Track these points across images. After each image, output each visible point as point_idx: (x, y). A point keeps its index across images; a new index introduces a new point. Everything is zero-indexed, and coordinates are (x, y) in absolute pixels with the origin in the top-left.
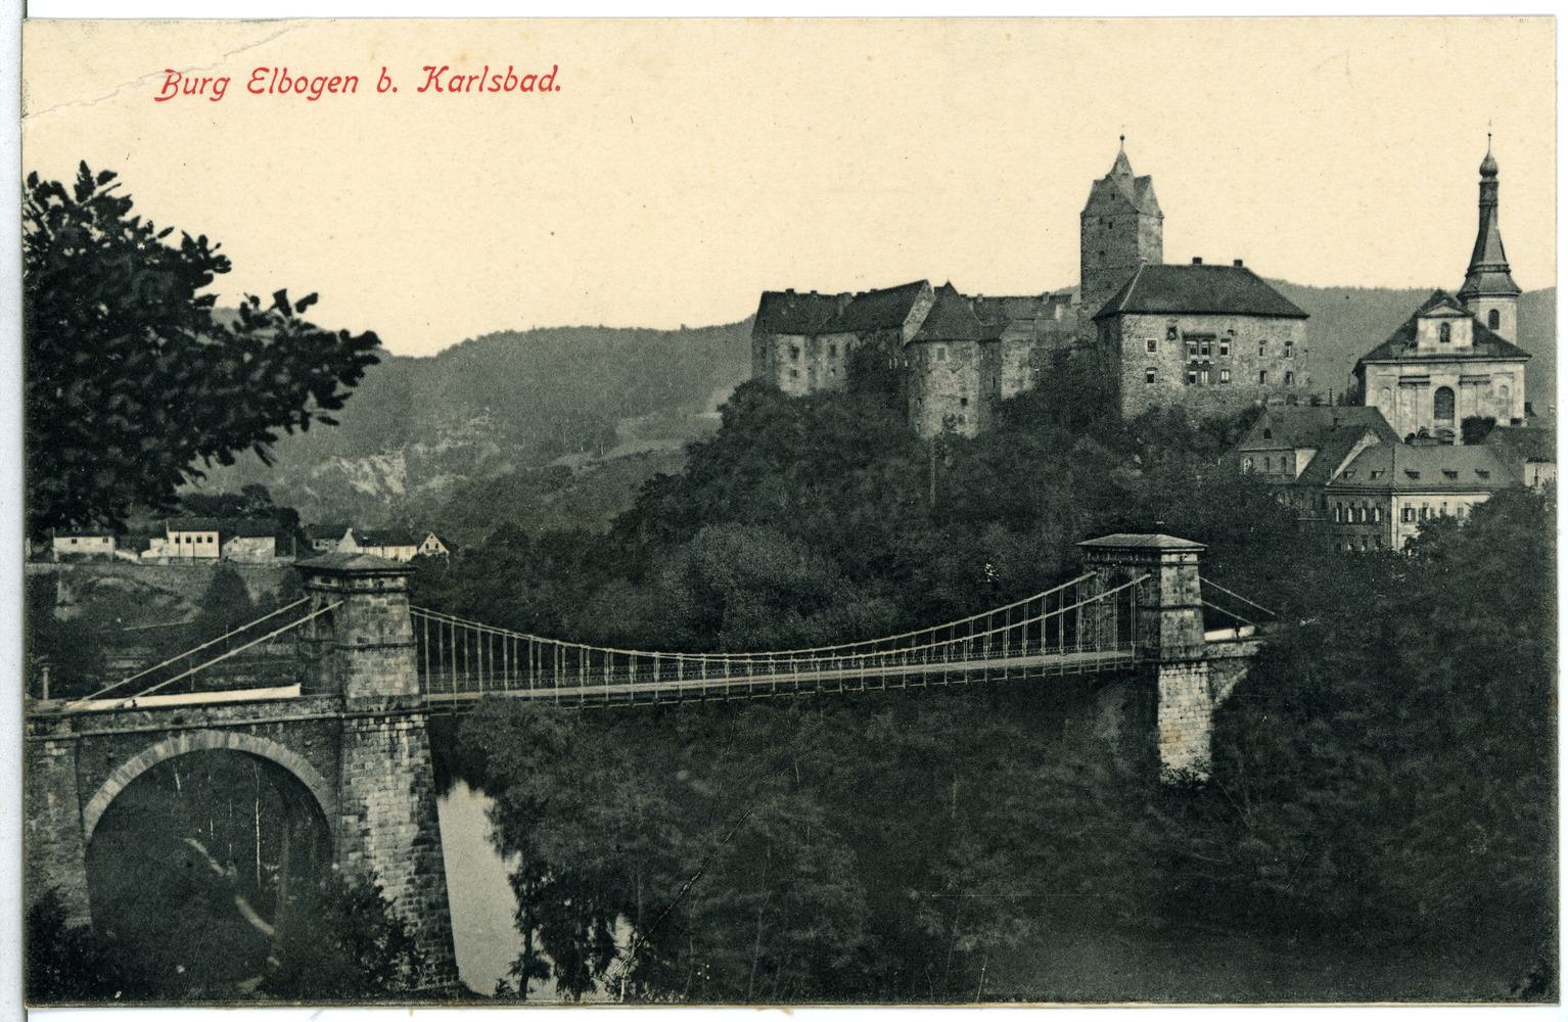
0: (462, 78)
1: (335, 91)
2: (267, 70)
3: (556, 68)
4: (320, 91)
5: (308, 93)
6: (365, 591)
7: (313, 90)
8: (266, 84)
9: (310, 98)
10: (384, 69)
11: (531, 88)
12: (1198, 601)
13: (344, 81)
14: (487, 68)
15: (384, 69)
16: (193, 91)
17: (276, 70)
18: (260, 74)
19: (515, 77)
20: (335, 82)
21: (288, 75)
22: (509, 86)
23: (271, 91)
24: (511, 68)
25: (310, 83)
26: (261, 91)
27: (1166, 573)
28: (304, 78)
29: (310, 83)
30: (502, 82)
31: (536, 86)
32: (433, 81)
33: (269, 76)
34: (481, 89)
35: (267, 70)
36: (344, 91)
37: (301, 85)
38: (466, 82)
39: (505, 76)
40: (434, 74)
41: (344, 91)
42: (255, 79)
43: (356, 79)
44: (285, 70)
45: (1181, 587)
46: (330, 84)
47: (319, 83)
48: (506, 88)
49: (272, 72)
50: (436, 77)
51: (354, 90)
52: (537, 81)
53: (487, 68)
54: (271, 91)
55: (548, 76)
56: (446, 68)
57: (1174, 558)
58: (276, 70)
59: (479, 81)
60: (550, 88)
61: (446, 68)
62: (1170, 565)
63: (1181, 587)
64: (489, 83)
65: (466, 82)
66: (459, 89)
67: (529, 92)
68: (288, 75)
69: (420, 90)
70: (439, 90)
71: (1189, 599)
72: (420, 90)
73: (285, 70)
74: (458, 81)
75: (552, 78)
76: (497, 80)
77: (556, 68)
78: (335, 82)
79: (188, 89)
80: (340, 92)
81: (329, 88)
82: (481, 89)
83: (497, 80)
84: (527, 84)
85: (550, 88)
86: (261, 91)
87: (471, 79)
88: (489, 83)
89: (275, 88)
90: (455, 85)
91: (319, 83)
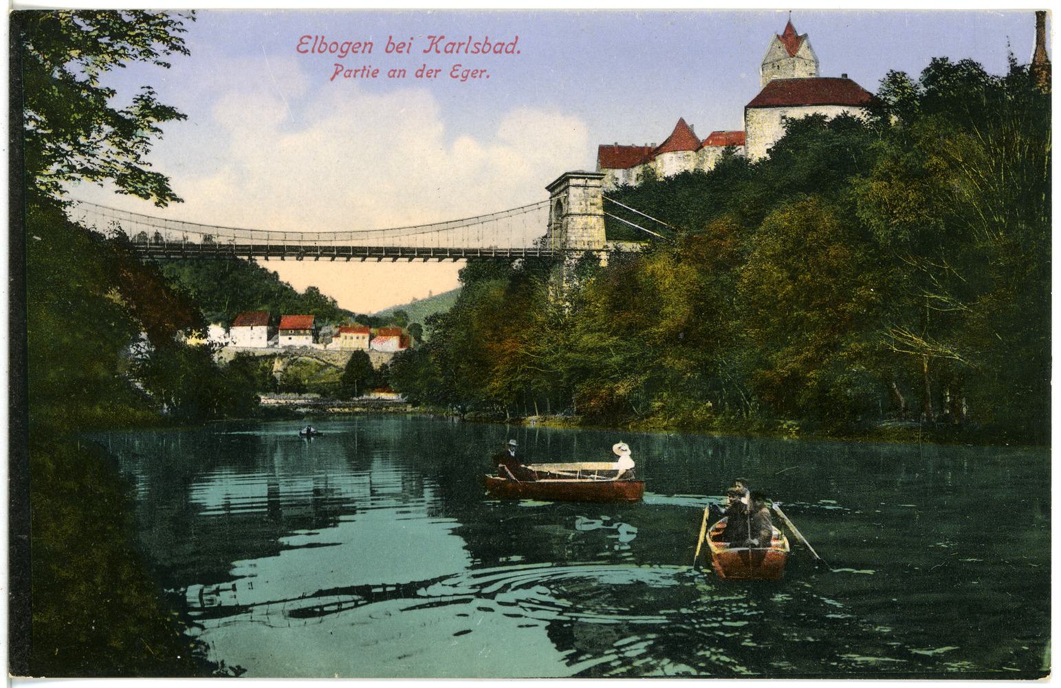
0: (454, 44)
1: (357, 52)
2: (310, 37)
3: (517, 38)
4: (347, 52)
5: (338, 52)
6: (304, 406)
7: (342, 51)
8: (309, 48)
9: (340, 56)
10: (391, 37)
11: (500, 52)
12: (601, 212)
13: (363, 45)
14: (470, 38)
15: (391, 37)
16: (400, 71)
17: (317, 37)
18: (305, 40)
19: (489, 44)
20: (402, 45)
21: (325, 41)
22: (485, 50)
23: (313, 51)
24: (487, 38)
25: (492, 49)
26: (306, 51)
27: (572, 190)
28: (336, 43)
29: (492, 49)
30: (480, 47)
31: (503, 50)
32: (434, 45)
33: (312, 42)
34: (466, 52)
35: (310, 37)
36: (363, 52)
37: (334, 47)
38: (456, 47)
39: (483, 44)
40: (435, 41)
41: (363, 52)
42: (302, 43)
43: (371, 44)
44: (323, 38)
45: (586, 201)
46: (472, 74)
47: (346, 46)
48: (483, 52)
49: (314, 39)
50: (436, 43)
51: (370, 52)
52: (505, 47)
53: (470, 38)
54: (313, 51)
55: (512, 44)
56: (442, 37)
57: (581, 182)
58: (317, 37)
59: (465, 46)
60: (512, 52)
61: (442, 37)
62: (577, 186)
63: (586, 201)
64: (472, 48)
65: (456, 47)
66: (451, 51)
67: (498, 54)
68: (325, 41)
69: (425, 51)
70: (438, 52)
71: (592, 209)
72: (425, 51)
73: (323, 38)
74: (451, 46)
75: (514, 44)
76: (477, 45)
77: (517, 38)
78: (358, 45)
79: (370, 45)
80: (432, 78)
81: (353, 51)
82: (466, 52)
83: (477, 45)
84: (498, 48)
85: (512, 52)
86: (306, 51)
87: (460, 45)
88: (472, 48)
89: (316, 49)
90: (449, 49)
91: (346, 46)
